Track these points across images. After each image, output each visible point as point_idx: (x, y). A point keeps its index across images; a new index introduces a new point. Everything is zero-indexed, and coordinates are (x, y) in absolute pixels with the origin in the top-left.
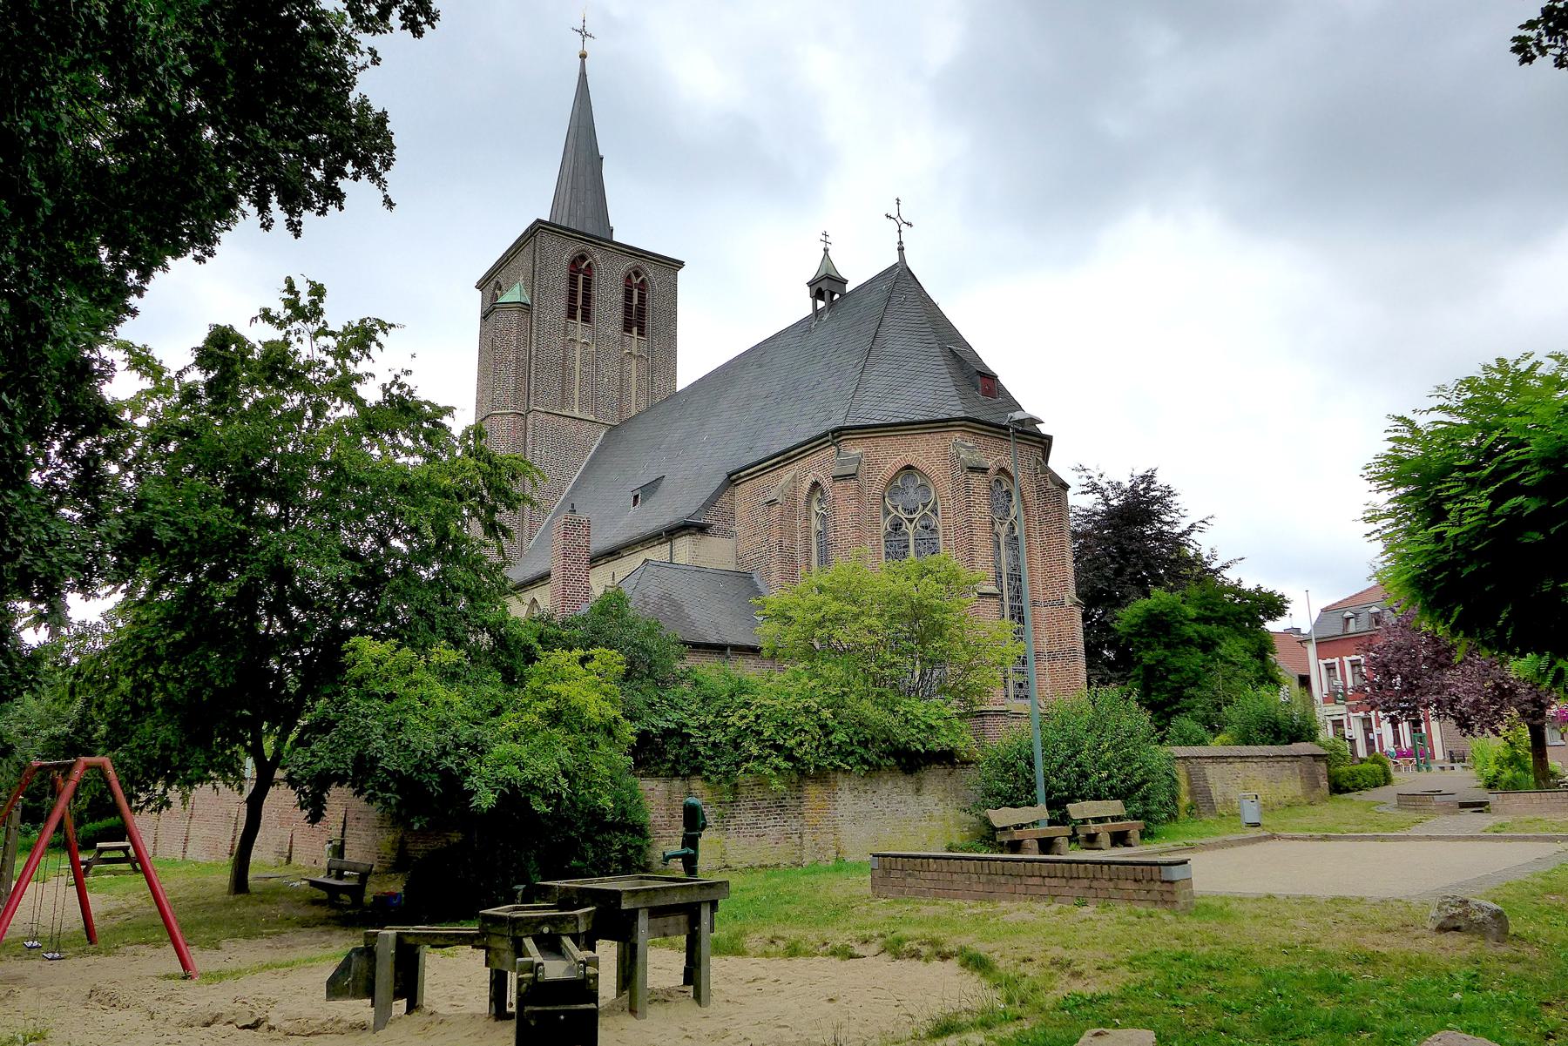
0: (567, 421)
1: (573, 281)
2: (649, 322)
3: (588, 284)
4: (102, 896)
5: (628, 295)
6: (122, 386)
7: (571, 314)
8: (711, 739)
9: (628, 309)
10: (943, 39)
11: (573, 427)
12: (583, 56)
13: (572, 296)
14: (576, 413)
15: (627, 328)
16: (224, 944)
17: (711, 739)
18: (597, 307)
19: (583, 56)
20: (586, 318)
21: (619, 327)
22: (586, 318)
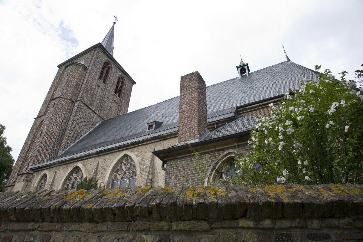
0: (90, 111)
1: (103, 68)
2: (122, 94)
3: (107, 72)
4: (322, 185)
5: (118, 83)
6: (272, 226)
7: (100, 78)
8: (196, 192)
9: (117, 87)
10: (338, 61)
11: (92, 114)
12: (115, 23)
13: (102, 73)
14: (94, 110)
15: (116, 92)
16: (96, 180)
17: (196, 192)
18: (109, 80)
19: (115, 23)
20: (104, 81)
21: (113, 92)
22: (104, 81)
